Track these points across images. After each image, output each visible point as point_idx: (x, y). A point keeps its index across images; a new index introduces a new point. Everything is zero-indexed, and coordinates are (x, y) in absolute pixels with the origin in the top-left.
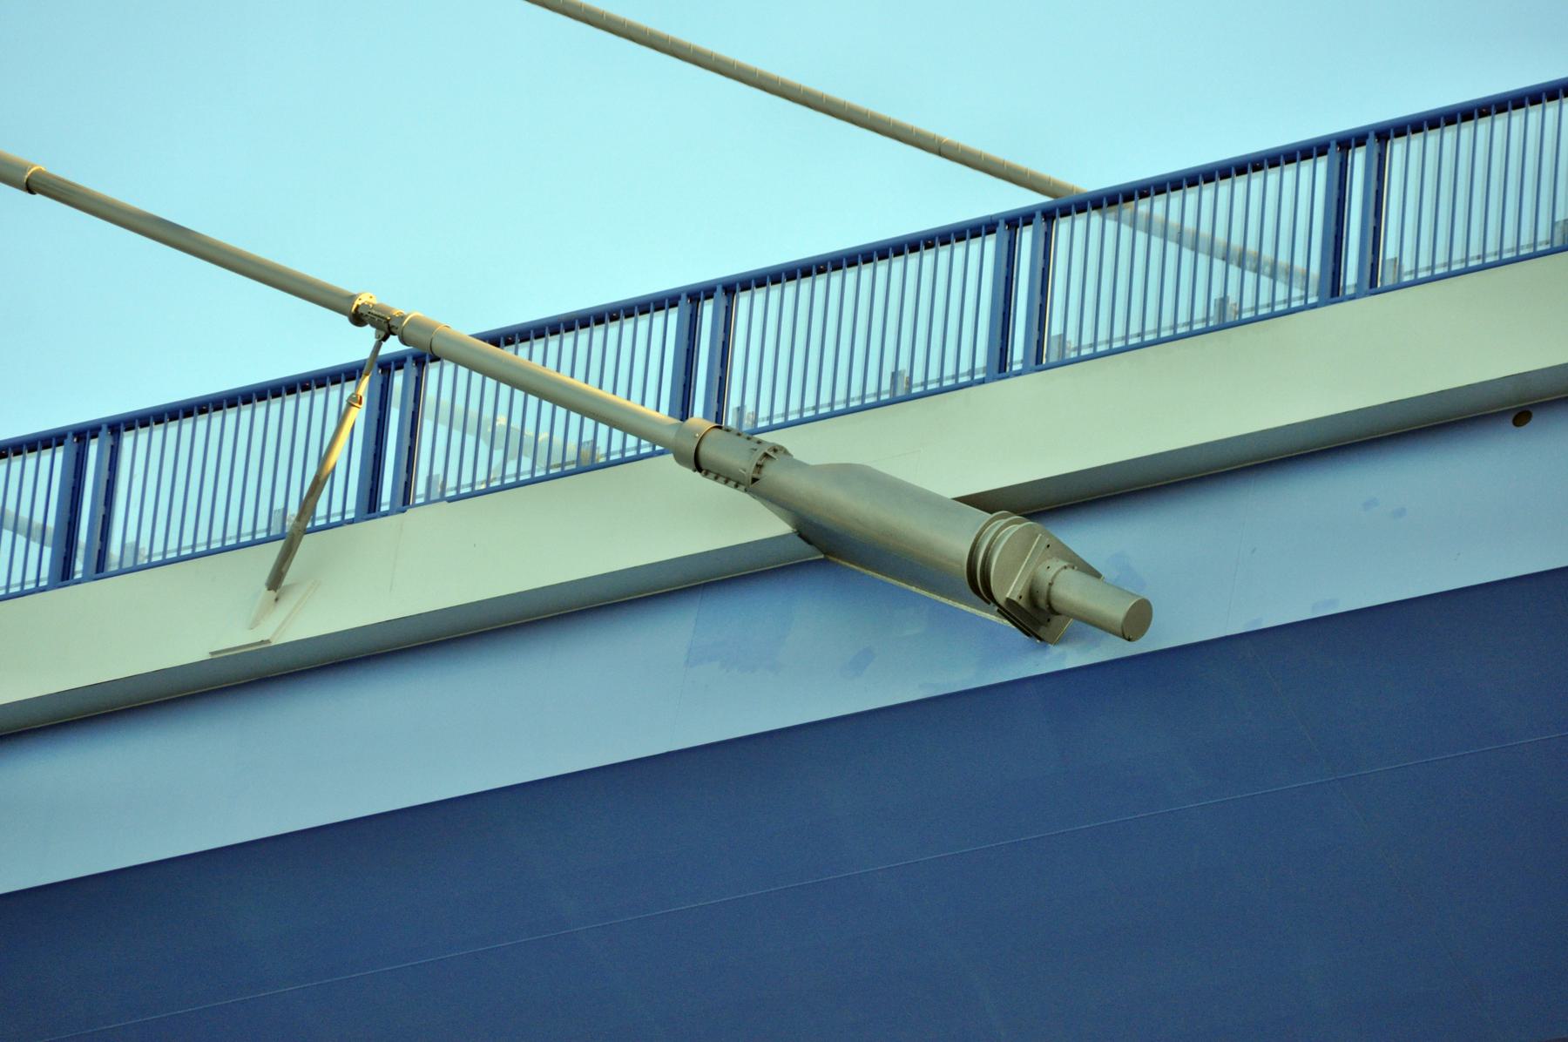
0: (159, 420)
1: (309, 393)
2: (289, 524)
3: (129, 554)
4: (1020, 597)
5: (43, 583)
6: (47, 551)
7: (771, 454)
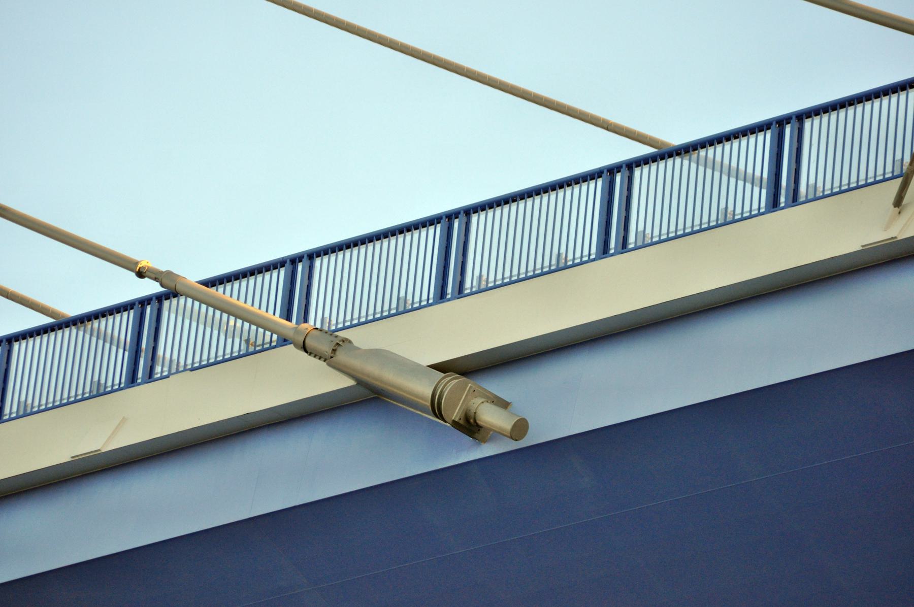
0: (393, 234)
1: (571, 187)
2: (905, 168)
3: (811, 190)
4: (460, 419)
5: (762, 210)
6: (764, 192)
7: (340, 343)
